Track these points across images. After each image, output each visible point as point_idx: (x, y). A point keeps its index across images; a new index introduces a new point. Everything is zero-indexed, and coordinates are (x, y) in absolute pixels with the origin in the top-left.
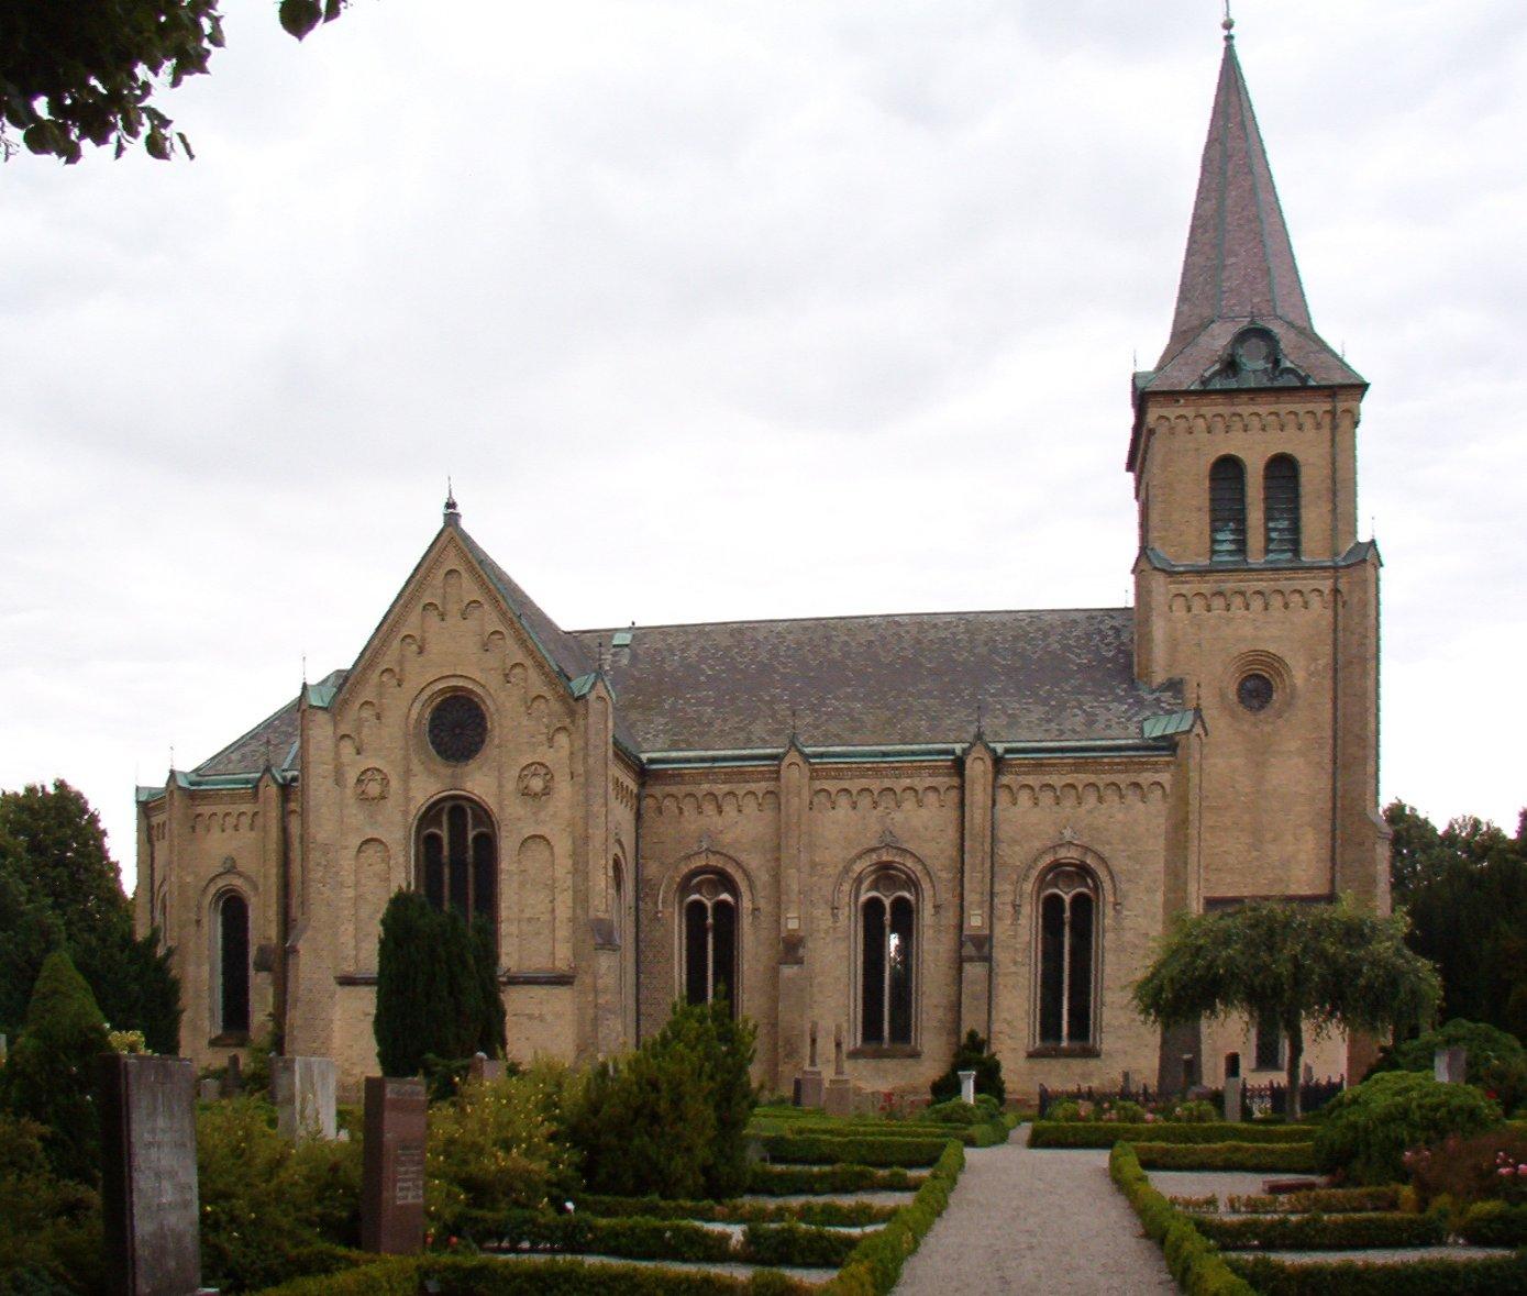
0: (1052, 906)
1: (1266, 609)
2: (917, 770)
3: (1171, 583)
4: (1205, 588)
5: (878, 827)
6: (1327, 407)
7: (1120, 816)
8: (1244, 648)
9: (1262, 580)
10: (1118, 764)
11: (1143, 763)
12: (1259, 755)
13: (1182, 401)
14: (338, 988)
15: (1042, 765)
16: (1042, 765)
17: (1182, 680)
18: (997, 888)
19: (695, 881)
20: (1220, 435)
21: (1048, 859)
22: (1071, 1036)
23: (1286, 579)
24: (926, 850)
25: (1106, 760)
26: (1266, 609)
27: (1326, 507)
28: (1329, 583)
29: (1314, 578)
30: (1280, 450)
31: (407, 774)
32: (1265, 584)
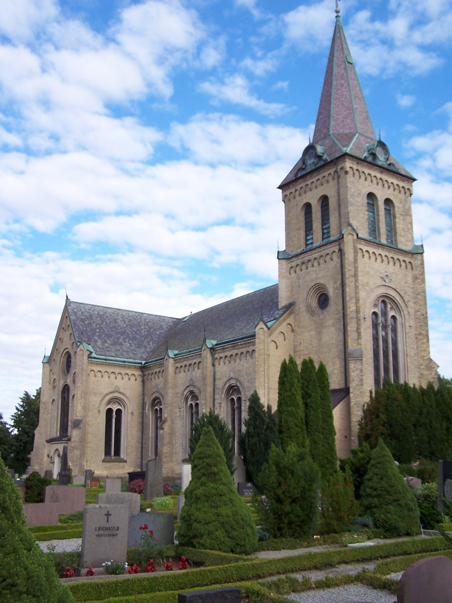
0: (109, 412)
1: (319, 265)
2: (129, 367)
3: (289, 263)
4: (299, 262)
5: (189, 378)
6: (334, 169)
7: (246, 365)
8: (313, 284)
9: (316, 253)
10: (243, 344)
11: (250, 343)
12: (319, 328)
13: (291, 186)
14: (46, 443)
15: (224, 349)
16: (224, 349)
17: (294, 302)
18: (216, 397)
19: (156, 402)
20: (303, 196)
21: (228, 385)
22: (115, 455)
23: (324, 250)
24: (128, 393)
25: (239, 343)
26: (319, 265)
27: (337, 214)
28: (337, 247)
29: (332, 247)
30: (322, 195)
31: (59, 379)
32: (317, 254)
